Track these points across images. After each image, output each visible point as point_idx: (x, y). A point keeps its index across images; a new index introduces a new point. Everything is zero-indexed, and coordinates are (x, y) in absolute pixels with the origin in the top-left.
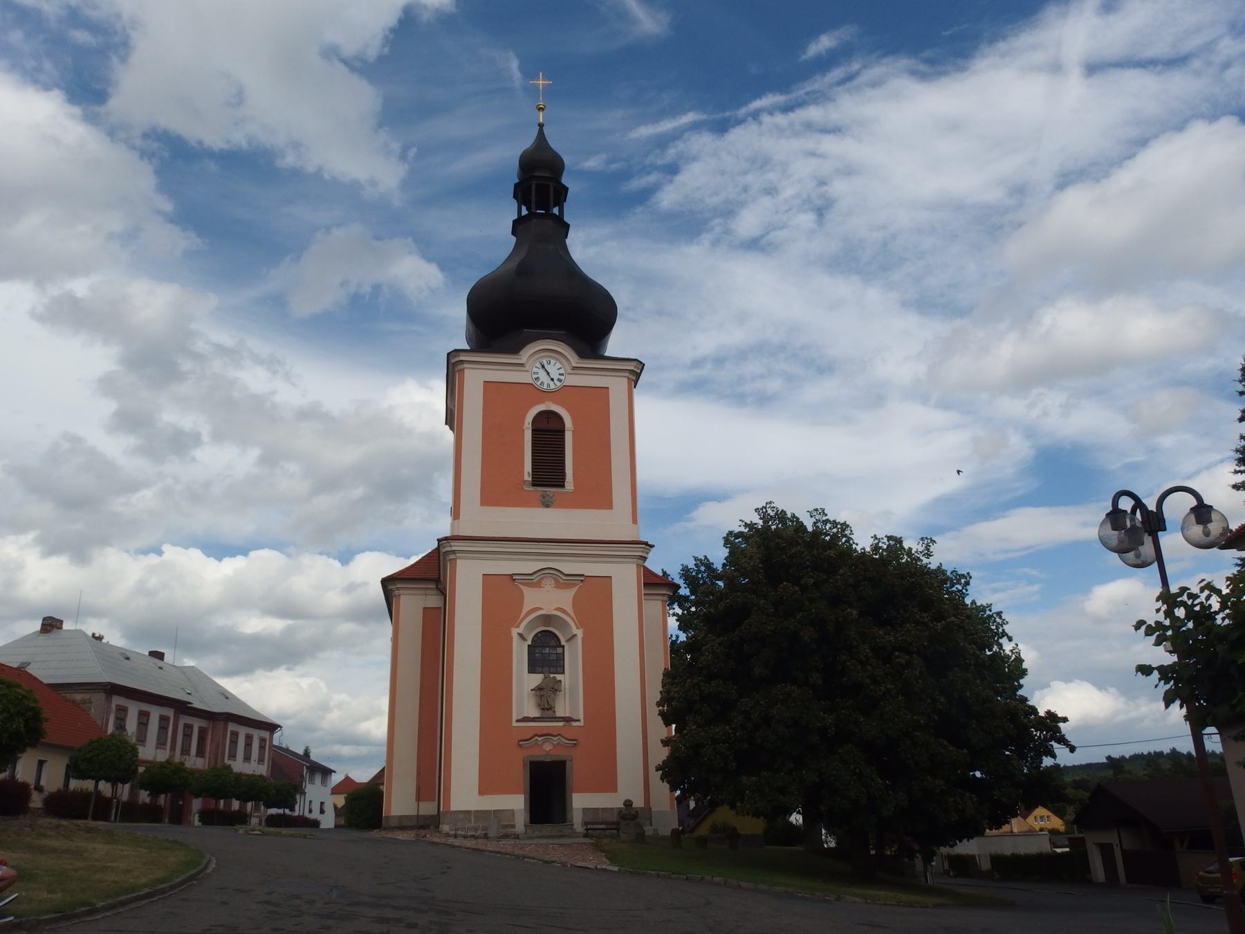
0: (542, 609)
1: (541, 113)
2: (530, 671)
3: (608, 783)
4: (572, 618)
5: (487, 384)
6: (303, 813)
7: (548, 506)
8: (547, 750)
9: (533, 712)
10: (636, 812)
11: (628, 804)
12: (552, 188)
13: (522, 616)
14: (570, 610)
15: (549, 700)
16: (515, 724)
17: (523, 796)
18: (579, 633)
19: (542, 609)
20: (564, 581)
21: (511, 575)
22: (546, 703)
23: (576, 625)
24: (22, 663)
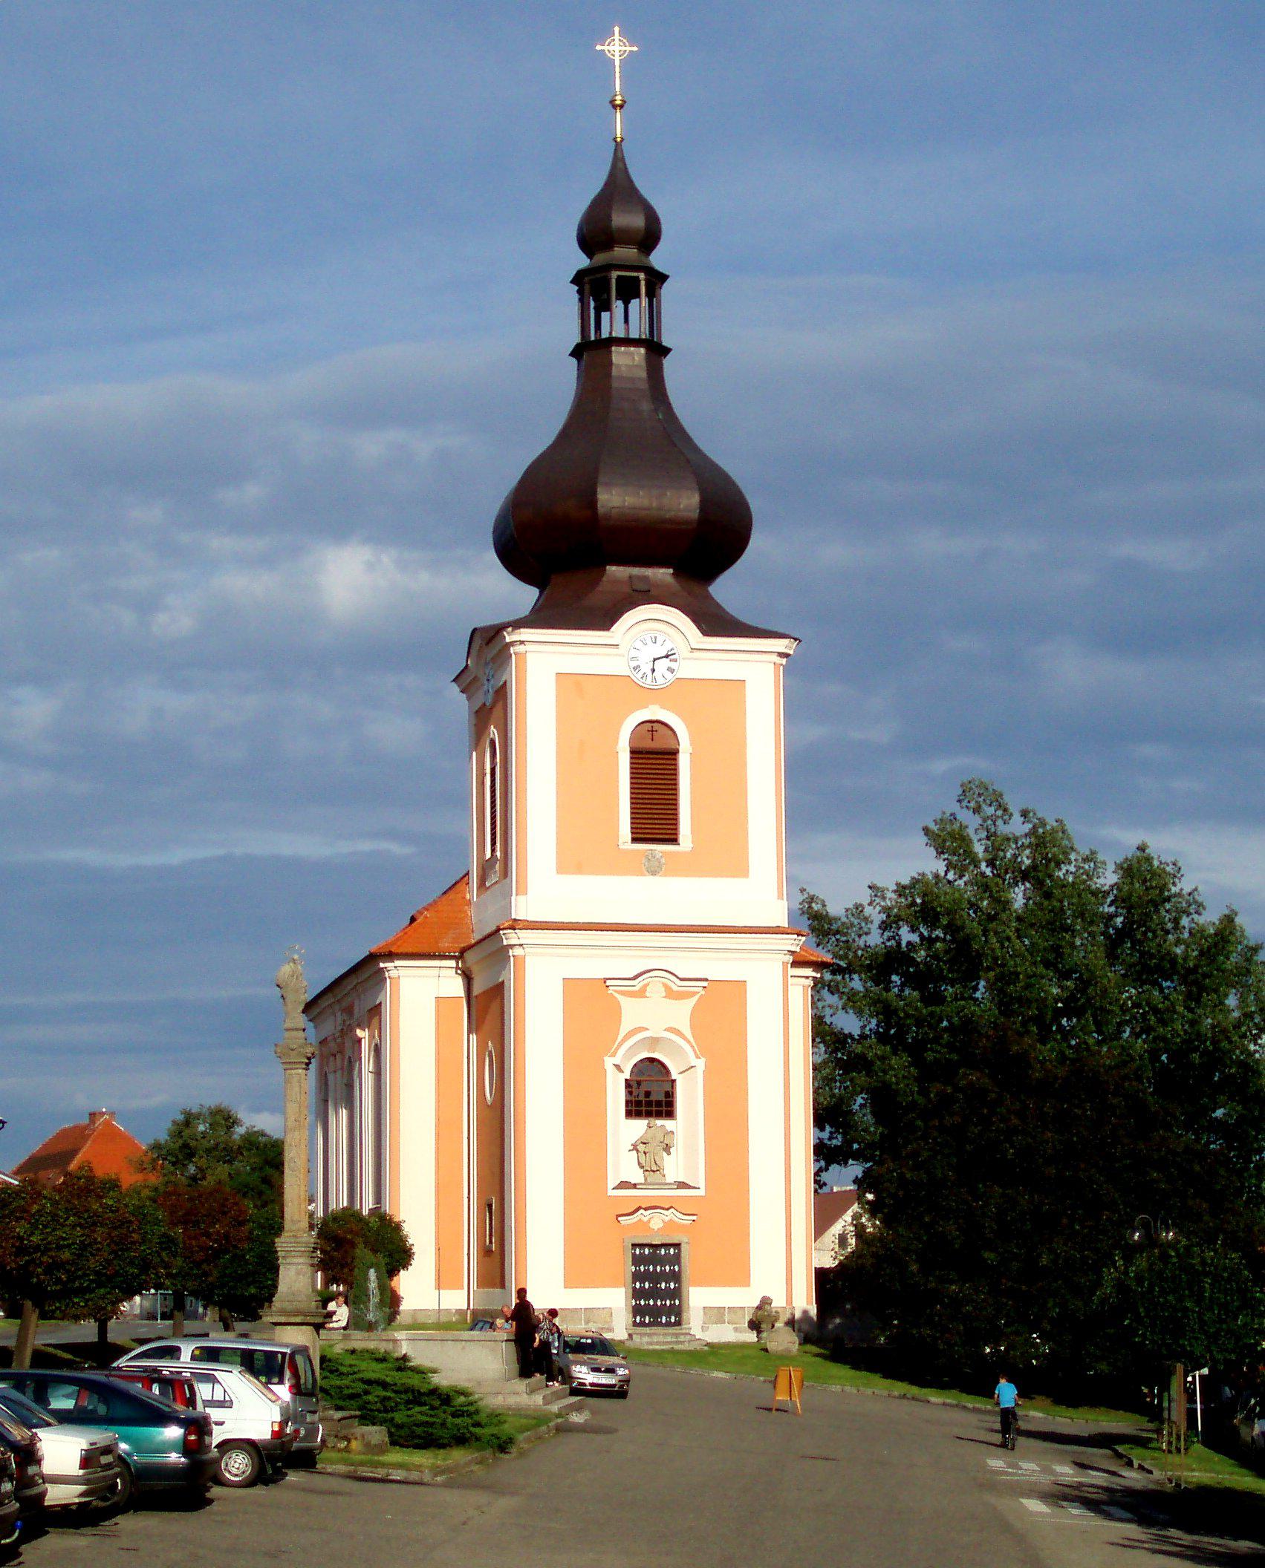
0: (647, 1029)
1: (618, 115)
2: (629, 1114)
3: (741, 1277)
4: (689, 1042)
5: (562, 868)
6: (378, 1197)
7: (654, 873)
8: (656, 1226)
9: (637, 1176)
10: (776, 1312)
11: (765, 1301)
12: (643, 283)
13: (620, 1038)
14: (687, 1032)
15: (656, 1158)
16: (611, 1193)
17: (623, 1290)
18: (700, 1064)
19: (647, 1029)
20: (677, 987)
21: (605, 980)
22: (653, 1163)
23: (695, 1053)
24: (64, 1134)
